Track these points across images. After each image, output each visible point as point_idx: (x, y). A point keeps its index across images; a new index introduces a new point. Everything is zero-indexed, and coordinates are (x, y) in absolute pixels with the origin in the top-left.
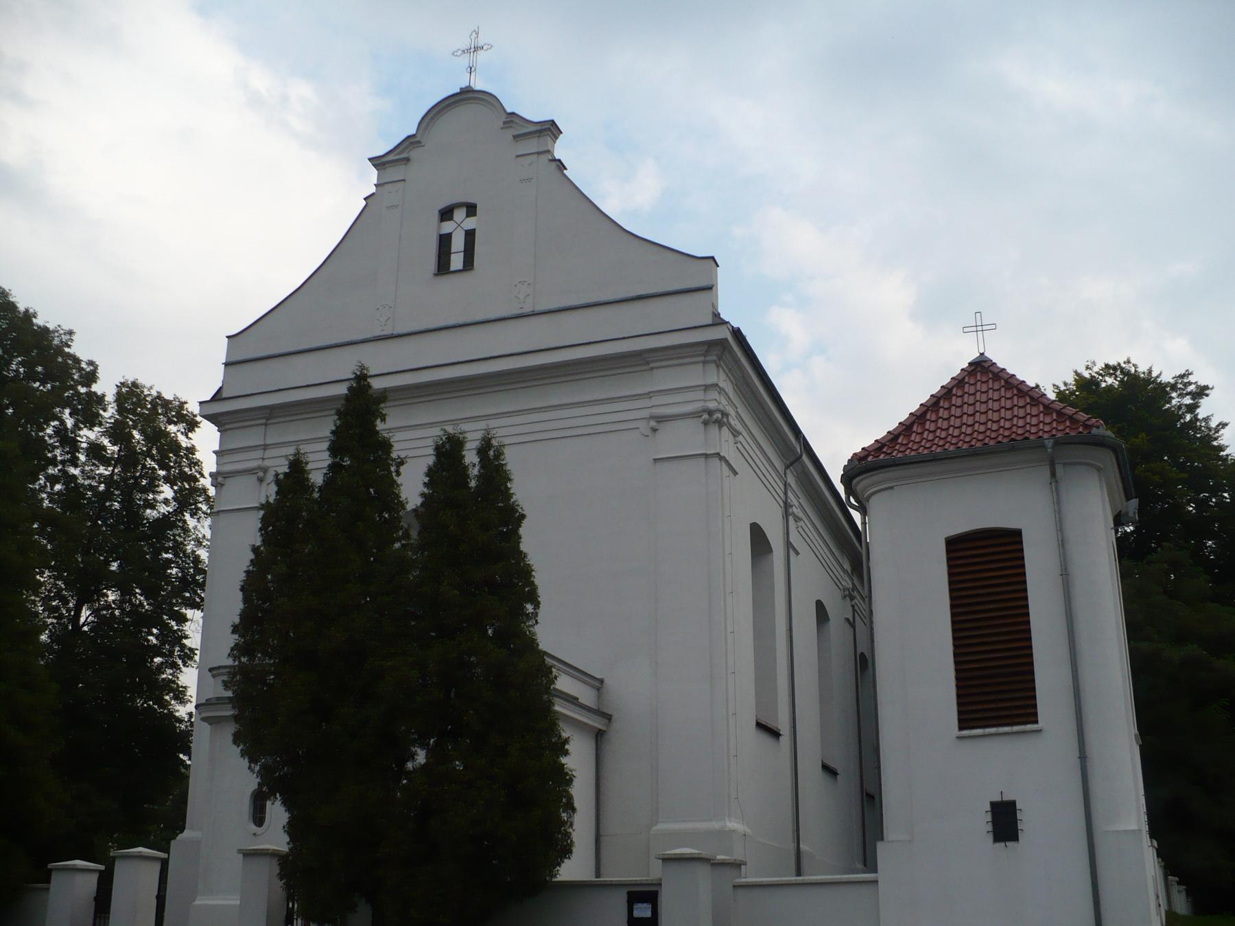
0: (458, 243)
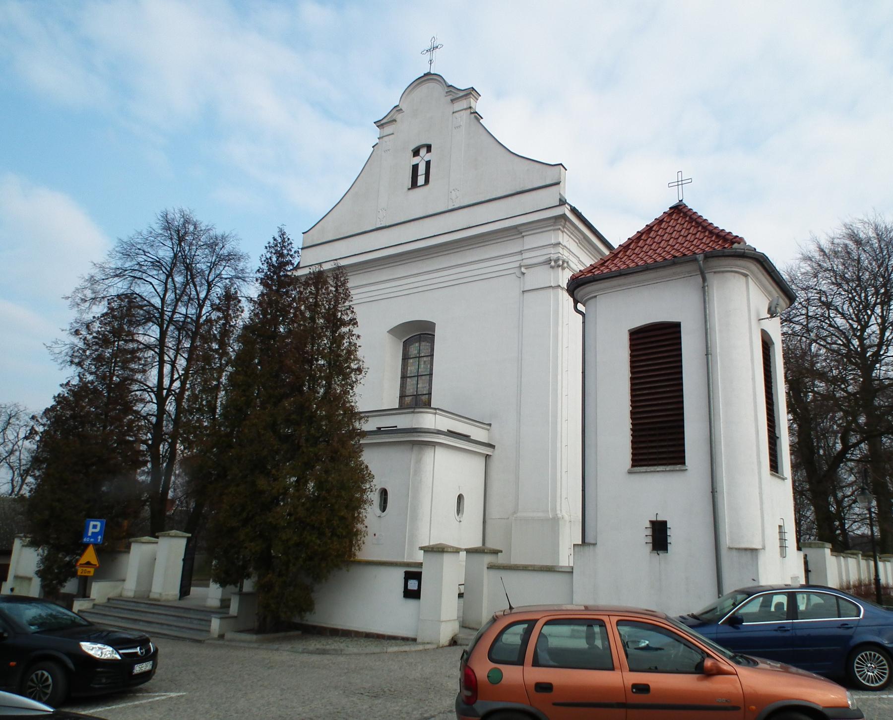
0: (422, 170)
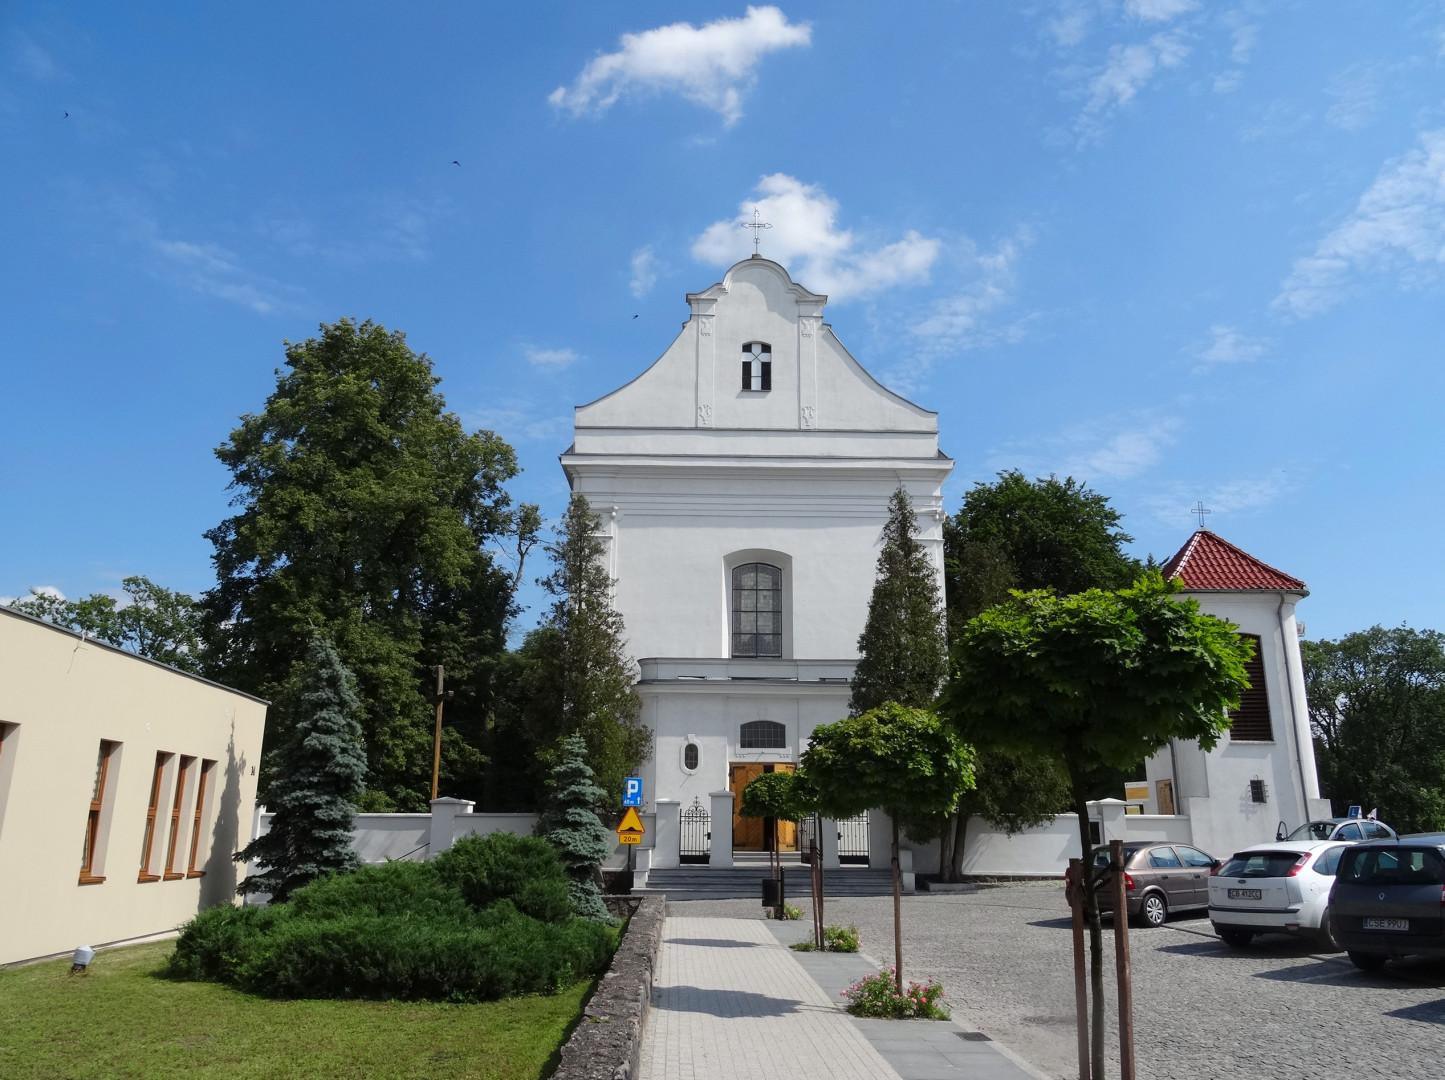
0: (756, 370)
